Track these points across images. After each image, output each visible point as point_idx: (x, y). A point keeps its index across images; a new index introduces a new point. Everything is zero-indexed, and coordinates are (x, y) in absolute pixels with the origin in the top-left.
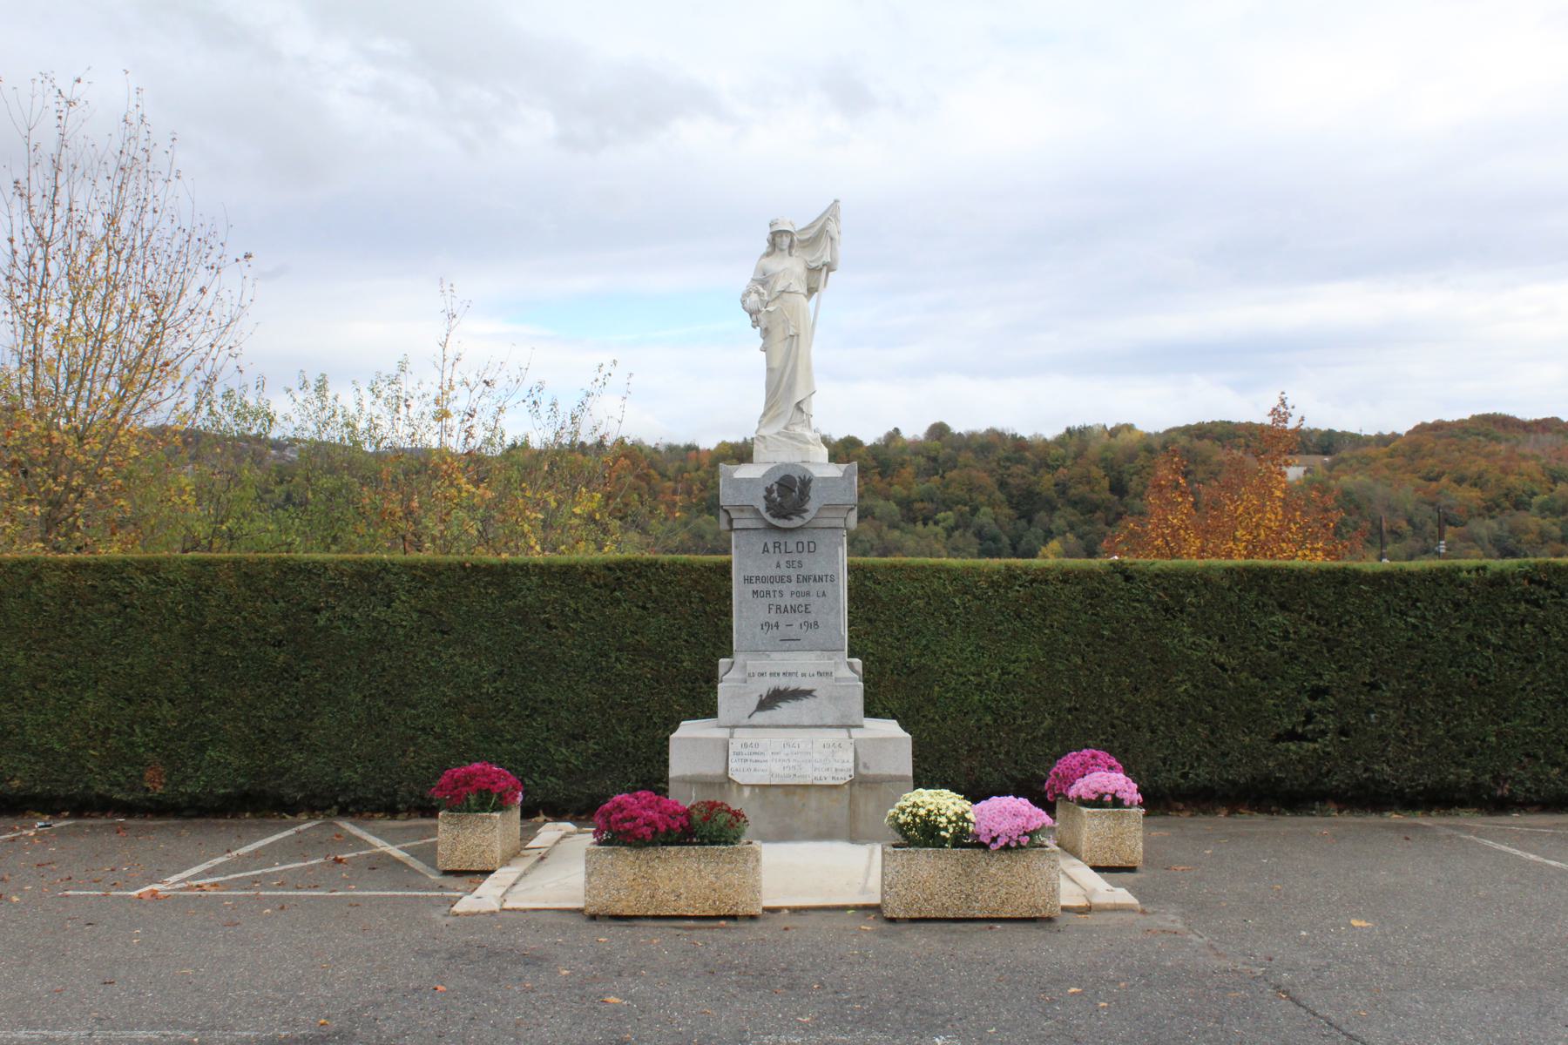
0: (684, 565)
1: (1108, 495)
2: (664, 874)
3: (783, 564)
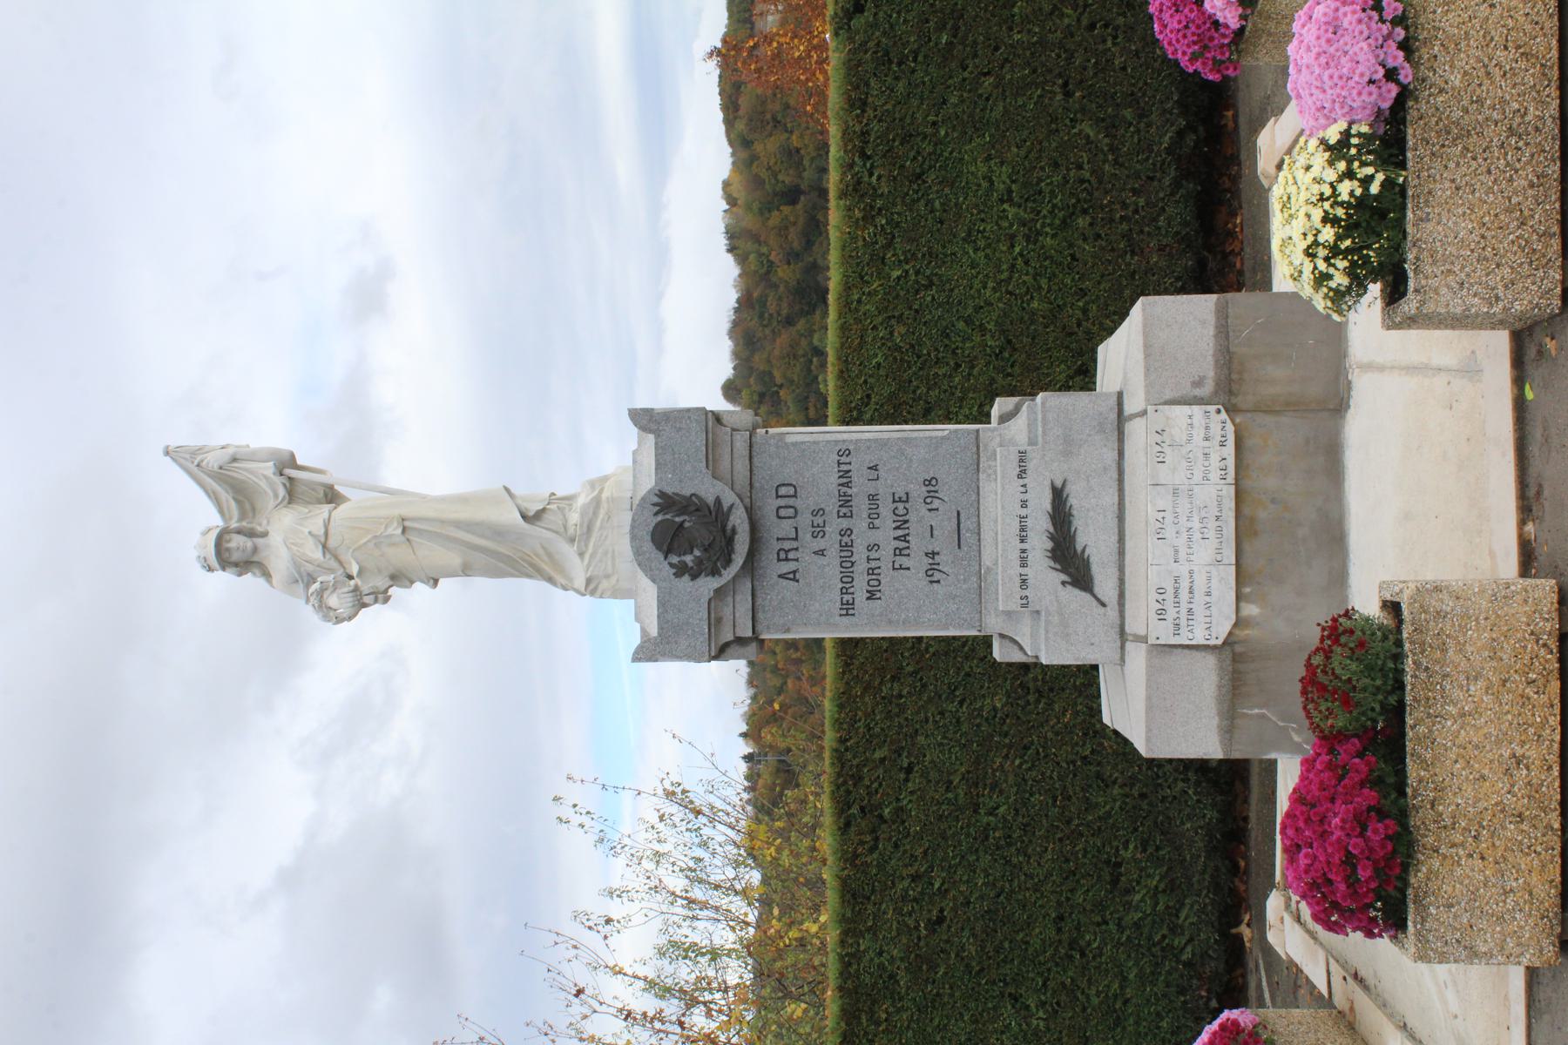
0: (841, 707)
1: (799, 206)
2: (1469, 791)
3: (820, 544)
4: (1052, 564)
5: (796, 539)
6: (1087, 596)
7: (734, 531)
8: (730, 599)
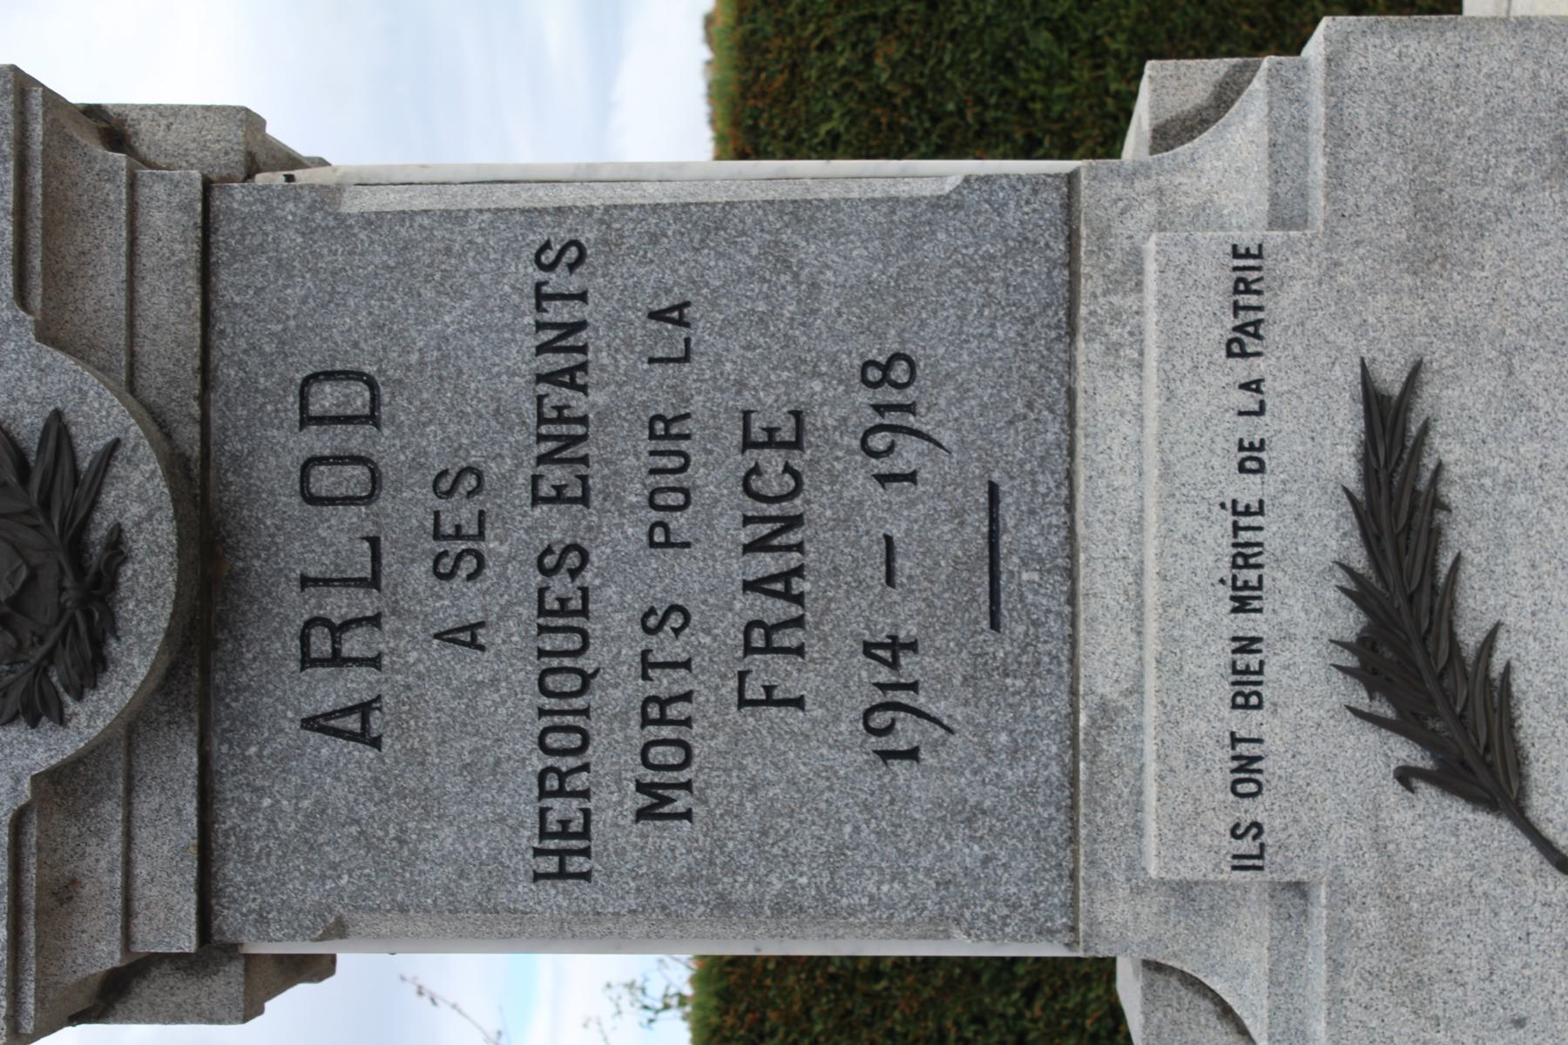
3: (463, 601)
4: (1361, 698)
5: (373, 582)
6: (1500, 830)
7: (117, 546)
8: (111, 810)
